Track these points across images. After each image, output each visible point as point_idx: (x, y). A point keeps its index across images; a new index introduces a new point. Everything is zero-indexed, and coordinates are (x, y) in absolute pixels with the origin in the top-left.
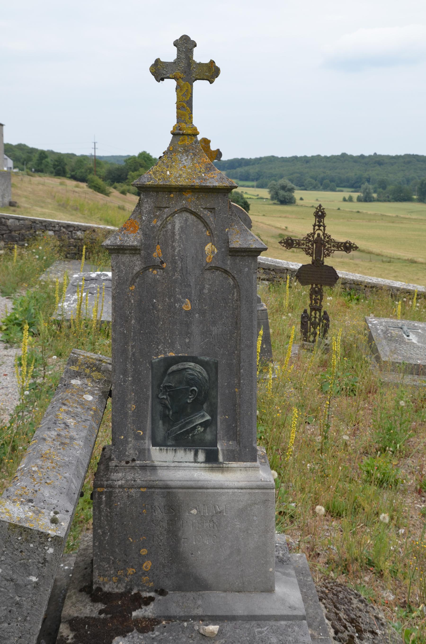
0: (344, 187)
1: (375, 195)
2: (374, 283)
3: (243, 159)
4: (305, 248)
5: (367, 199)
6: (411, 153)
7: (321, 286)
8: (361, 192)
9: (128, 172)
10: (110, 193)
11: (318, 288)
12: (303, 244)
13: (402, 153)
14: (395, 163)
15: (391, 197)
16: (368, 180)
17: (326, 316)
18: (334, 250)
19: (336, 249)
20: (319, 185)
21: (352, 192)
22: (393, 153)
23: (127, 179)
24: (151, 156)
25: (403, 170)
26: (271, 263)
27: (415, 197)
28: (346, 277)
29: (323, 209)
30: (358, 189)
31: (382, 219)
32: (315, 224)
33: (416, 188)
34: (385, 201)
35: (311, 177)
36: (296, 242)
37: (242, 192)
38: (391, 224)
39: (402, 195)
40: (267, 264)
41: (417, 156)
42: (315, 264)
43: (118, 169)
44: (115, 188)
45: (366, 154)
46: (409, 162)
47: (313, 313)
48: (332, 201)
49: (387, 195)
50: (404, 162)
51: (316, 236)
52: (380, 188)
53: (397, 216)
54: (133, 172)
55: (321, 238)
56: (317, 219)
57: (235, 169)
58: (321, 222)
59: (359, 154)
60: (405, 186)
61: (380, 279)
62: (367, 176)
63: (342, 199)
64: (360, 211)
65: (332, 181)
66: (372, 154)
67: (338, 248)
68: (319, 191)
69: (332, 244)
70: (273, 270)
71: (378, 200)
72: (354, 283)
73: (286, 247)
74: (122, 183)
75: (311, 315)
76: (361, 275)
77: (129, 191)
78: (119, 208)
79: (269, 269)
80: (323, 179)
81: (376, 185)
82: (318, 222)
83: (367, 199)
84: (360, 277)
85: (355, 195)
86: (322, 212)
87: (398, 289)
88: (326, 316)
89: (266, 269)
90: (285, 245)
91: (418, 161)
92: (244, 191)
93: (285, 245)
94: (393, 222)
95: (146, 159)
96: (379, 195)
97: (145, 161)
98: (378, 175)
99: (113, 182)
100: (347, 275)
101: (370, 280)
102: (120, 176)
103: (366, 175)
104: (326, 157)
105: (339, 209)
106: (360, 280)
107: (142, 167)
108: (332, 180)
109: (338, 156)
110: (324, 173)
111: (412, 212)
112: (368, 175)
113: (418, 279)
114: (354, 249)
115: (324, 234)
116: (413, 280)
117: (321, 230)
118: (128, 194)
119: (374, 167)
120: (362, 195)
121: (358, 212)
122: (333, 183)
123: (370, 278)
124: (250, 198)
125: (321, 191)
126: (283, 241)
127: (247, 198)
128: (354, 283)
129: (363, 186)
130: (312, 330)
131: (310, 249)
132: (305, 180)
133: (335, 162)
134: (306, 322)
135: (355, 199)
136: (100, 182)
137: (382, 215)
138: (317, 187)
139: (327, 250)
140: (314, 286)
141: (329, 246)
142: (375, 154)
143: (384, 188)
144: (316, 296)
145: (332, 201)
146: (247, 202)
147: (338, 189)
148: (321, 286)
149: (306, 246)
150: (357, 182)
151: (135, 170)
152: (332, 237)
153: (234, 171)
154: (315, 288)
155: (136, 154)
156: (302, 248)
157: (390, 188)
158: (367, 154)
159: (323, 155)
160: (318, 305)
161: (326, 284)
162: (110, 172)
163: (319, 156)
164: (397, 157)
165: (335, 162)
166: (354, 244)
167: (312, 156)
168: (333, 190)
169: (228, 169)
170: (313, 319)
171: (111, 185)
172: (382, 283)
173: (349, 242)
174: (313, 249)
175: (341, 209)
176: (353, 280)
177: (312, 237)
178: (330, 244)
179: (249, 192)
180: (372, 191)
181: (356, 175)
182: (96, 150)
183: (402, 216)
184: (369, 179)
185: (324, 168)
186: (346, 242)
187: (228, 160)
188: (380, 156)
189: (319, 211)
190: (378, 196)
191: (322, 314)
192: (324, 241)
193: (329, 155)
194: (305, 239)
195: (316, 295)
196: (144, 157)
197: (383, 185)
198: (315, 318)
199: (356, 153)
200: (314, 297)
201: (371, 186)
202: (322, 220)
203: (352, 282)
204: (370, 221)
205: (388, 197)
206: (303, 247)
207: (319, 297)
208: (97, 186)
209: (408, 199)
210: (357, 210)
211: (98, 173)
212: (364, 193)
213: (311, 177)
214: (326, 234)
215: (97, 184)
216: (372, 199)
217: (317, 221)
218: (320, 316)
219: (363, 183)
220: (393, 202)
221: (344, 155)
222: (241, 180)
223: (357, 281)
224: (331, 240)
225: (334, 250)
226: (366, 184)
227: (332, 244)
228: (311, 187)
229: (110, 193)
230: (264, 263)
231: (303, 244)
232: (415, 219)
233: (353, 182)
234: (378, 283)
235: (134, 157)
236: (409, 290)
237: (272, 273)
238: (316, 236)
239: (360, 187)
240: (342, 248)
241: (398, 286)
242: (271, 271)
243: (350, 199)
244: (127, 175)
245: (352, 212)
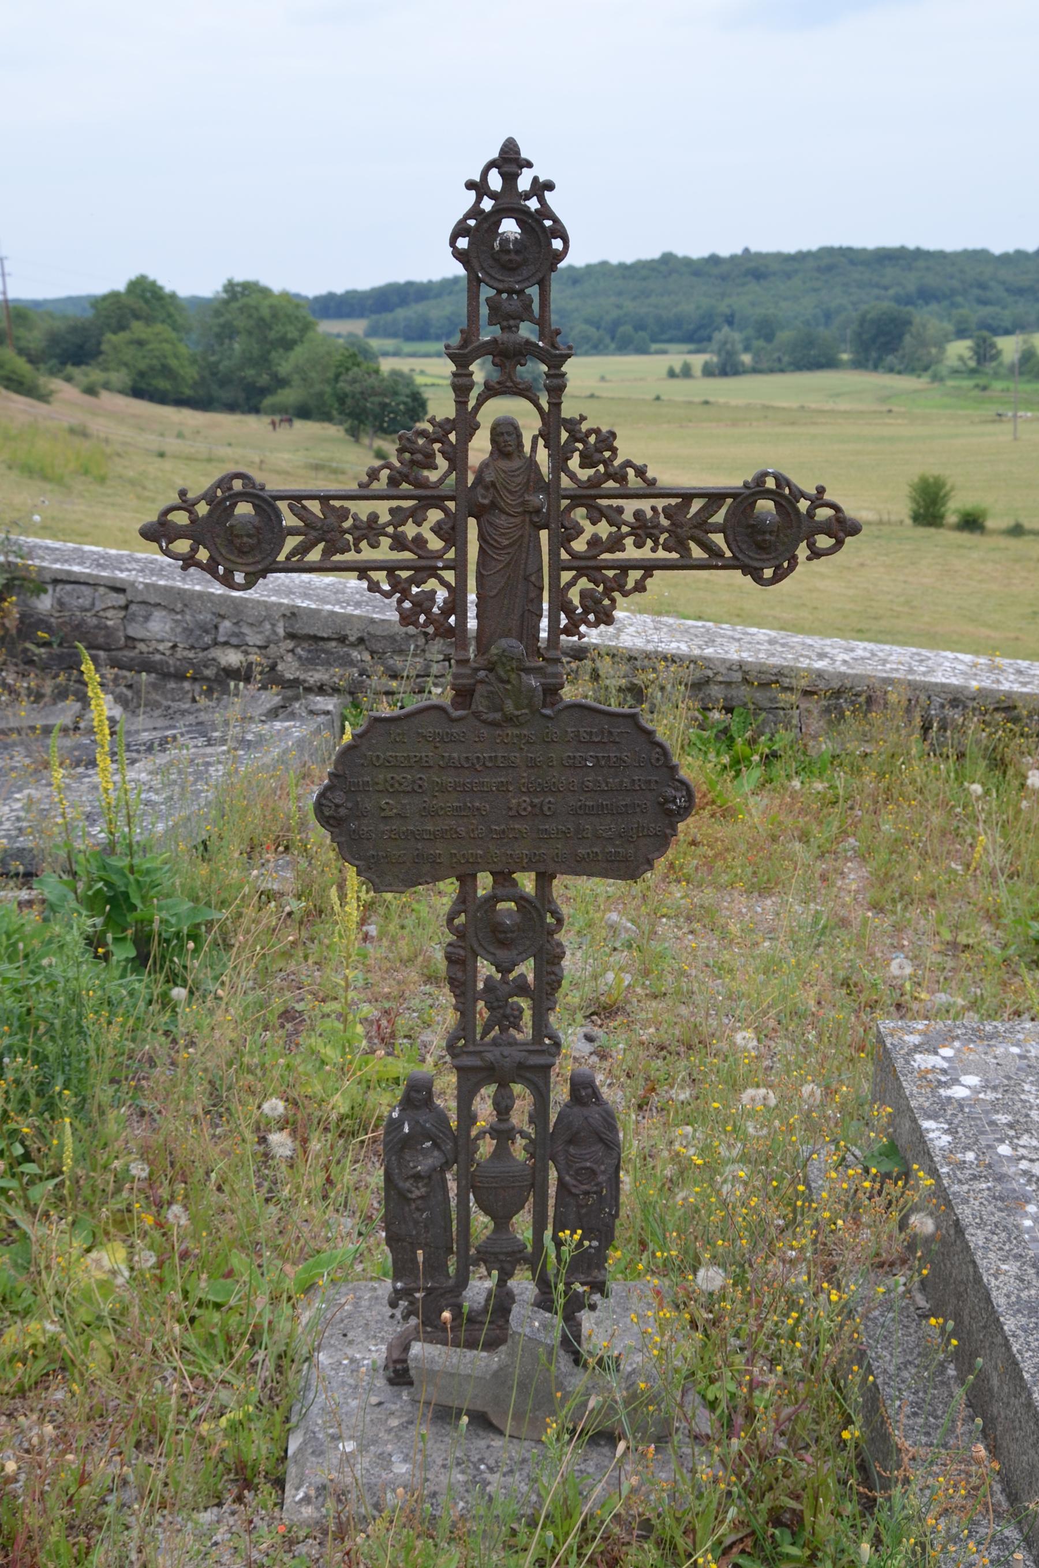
0: (670, 341)
1: (746, 358)
2: (843, 676)
3: (410, 284)
4: (391, 569)
5: (728, 369)
6: (836, 243)
7: (544, 880)
8: (712, 352)
9: (102, 334)
10: (51, 393)
11: (521, 900)
12: (370, 530)
13: (812, 244)
14: (796, 271)
15: (786, 359)
16: (730, 320)
17: (594, 1113)
18: (649, 568)
19: (661, 554)
20: (607, 340)
21: (690, 352)
22: (790, 247)
23: (100, 353)
24: (161, 288)
25: (816, 290)
26: (350, 610)
27: (845, 357)
28: (709, 651)
29: (541, 188)
30: (705, 344)
31: (766, 417)
32: (469, 335)
33: (849, 332)
34: (771, 371)
35: (588, 321)
36: (301, 513)
37: (412, 370)
38: (789, 429)
39: (812, 352)
40: (332, 613)
41: (850, 250)
42: (479, 703)
43: (74, 330)
44: (69, 379)
45: (724, 252)
46: (830, 268)
47: (484, 1108)
48: (641, 379)
49: (776, 355)
50: (819, 269)
51: (480, 447)
52: (758, 338)
53: (802, 407)
54: (115, 332)
55: (532, 464)
56: (486, 292)
57: (391, 310)
58: (524, 313)
59: (706, 254)
60: (821, 329)
61: (862, 648)
62: (728, 311)
63: (664, 372)
64: (711, 399)
65: (639, 327)
66: (739, 251)
67: (678, 544)
68: (607, 354)
69: (628, 516)
70: (361, 640)
71: (755, 370)
72: (746, 681)
73: (210, 568)
74: (87, 364)
75: (467, 1117)
76: (773, 634)
77: (107, 386)
78: (72, 431)
79: (342, 640)
80: (617, 323)
81: (750, 332)
82: (497, 314)
83: (728, 368)
84: (772, 642)
85: (698, 361)
86: (530, 222)
87: (957, 699)
88: (594, 1113)
89: (329, 639)
90: (203, 555)
91: (852, 262)
92: (418, 368)
93: (203, 555)
94: (793, 424)
95: (148, 295)
96: (757, 356)
97: (147, 301)
98: (753, 304)
99: (64, 363)
100: (711, 642)
101: (822, 656)
102: (81, 347)
103: (723, 308)
104: (622, 267)
105: (658, 398)
106: (773, 661)
107: (137, 317)
108: (640, 326)
109: (653, 261)
110: (619, 307)
111: (838, 395)
112: (729, 306)
113: (862, 565)
114: (823, 541)
115: (548, 435)
116: (849, 568)
117: (526, 392)
118: (105, 395)
119: (743, 285)
120: (715, 359)
121: (706, 403)
122: (641, 334)
123: (815, 642)
124: (433, 385)
125: (613, 354)
126: (181, 518)
127: (426, 385)
128: (746, 681)
129: (718, 336)
130: (481, 1222)
131: (433, 572)
132: (572, 329)
133: (644, 279)
134: (434, 1180)
135: (697, 370)
136: (22, 365)
137: (766, 408)
138: (601, 347)
139: (581, 572)
140: (484, 883)
141: (604, 529)
142: (746, 250)
143: (769, 338)
144: (504, 969)
145: (641, 379)
146: (418, 393)
147: (654, 347)
148: (544, 880)
149: (399, 543)
150: (701, 327)
151: (122, 327)
152: (626, 449)
153: (388, 317)
154: (493, 899)
155: (121, 286)
156: (362, 571)
157: (784, 336)
158: (724, 252)
159: (614, 261)
160: (525, 1033)
161: (583, 867)
162: (54, 339)
163: (604, 264)
164: (801, 257)
165: (644, 279)
166: (818, 499)
167: (589, 267)
168: (642, 351)
169: (374, 312)
170: (486, 1147)
171: (52, 373)
172: (881, 672)
173: (779, 479)
174: (459, 566)
175: (663, 397)
176: (741, 665)
177: (442, 463)
178: (614, 516)
179: (429, 370)
180: (740, 347)
181: (698, 308)
182: (8, 279)
183: (813, 406)
184: (732, 316)
185: (620, 294)
186: (756, 489)
187: (373, 290)
188: (759, 255)
189: (499, 213)
190: (753, 358)
191: (560, 1094)
192: (551, 488)
193: (629, 260)
194: (381, 484)
195: (502, 954)
196: (144, 291)
197: (766, 330)
198: (503, 1134)
199: (697, 251)
200: (485, 969)
201: (737, 336)
202: (534, 291)
203: (738, 676)
204: (735, 423)
205: (779, 360)
206: (368, 554)
207: (527, 969)
208: (14, 377)
209: (827, 363)
210: (702, 399)
211: (23, 344)
212: (719, 353)
213: (588, 321)
214: (572, 426)
215: (14, 372)
216: (741, 369)
217: (484, 311)
218: (540, 1114)
219: (718, 329)
220: (793, 371)
221: (668, 259)
222: (408, 338)
223: (762, 670)
224: (621, 478)
225: (649, 568)
226: (726, 329)
227: (628, 516)
228: (586, 347)
229: (51, 393)
230: (317, 612)
231: (370, 530)
232: (846, 412)
233: (692, 327)
234: (859, 670)
235: (114, 295)
236: (1009, 695)
237: (355, 654)
238: (480, 447)
239: (709, 339)
240: (718, 539)
241: (954, 681)
242: (353, 645)
243: (686, 372)
244: (99, 343)
245: (690, 403)
